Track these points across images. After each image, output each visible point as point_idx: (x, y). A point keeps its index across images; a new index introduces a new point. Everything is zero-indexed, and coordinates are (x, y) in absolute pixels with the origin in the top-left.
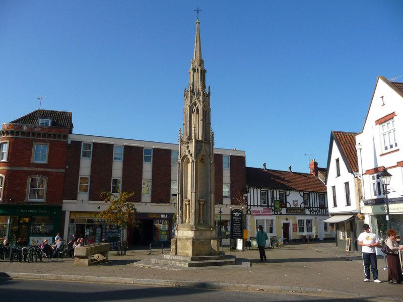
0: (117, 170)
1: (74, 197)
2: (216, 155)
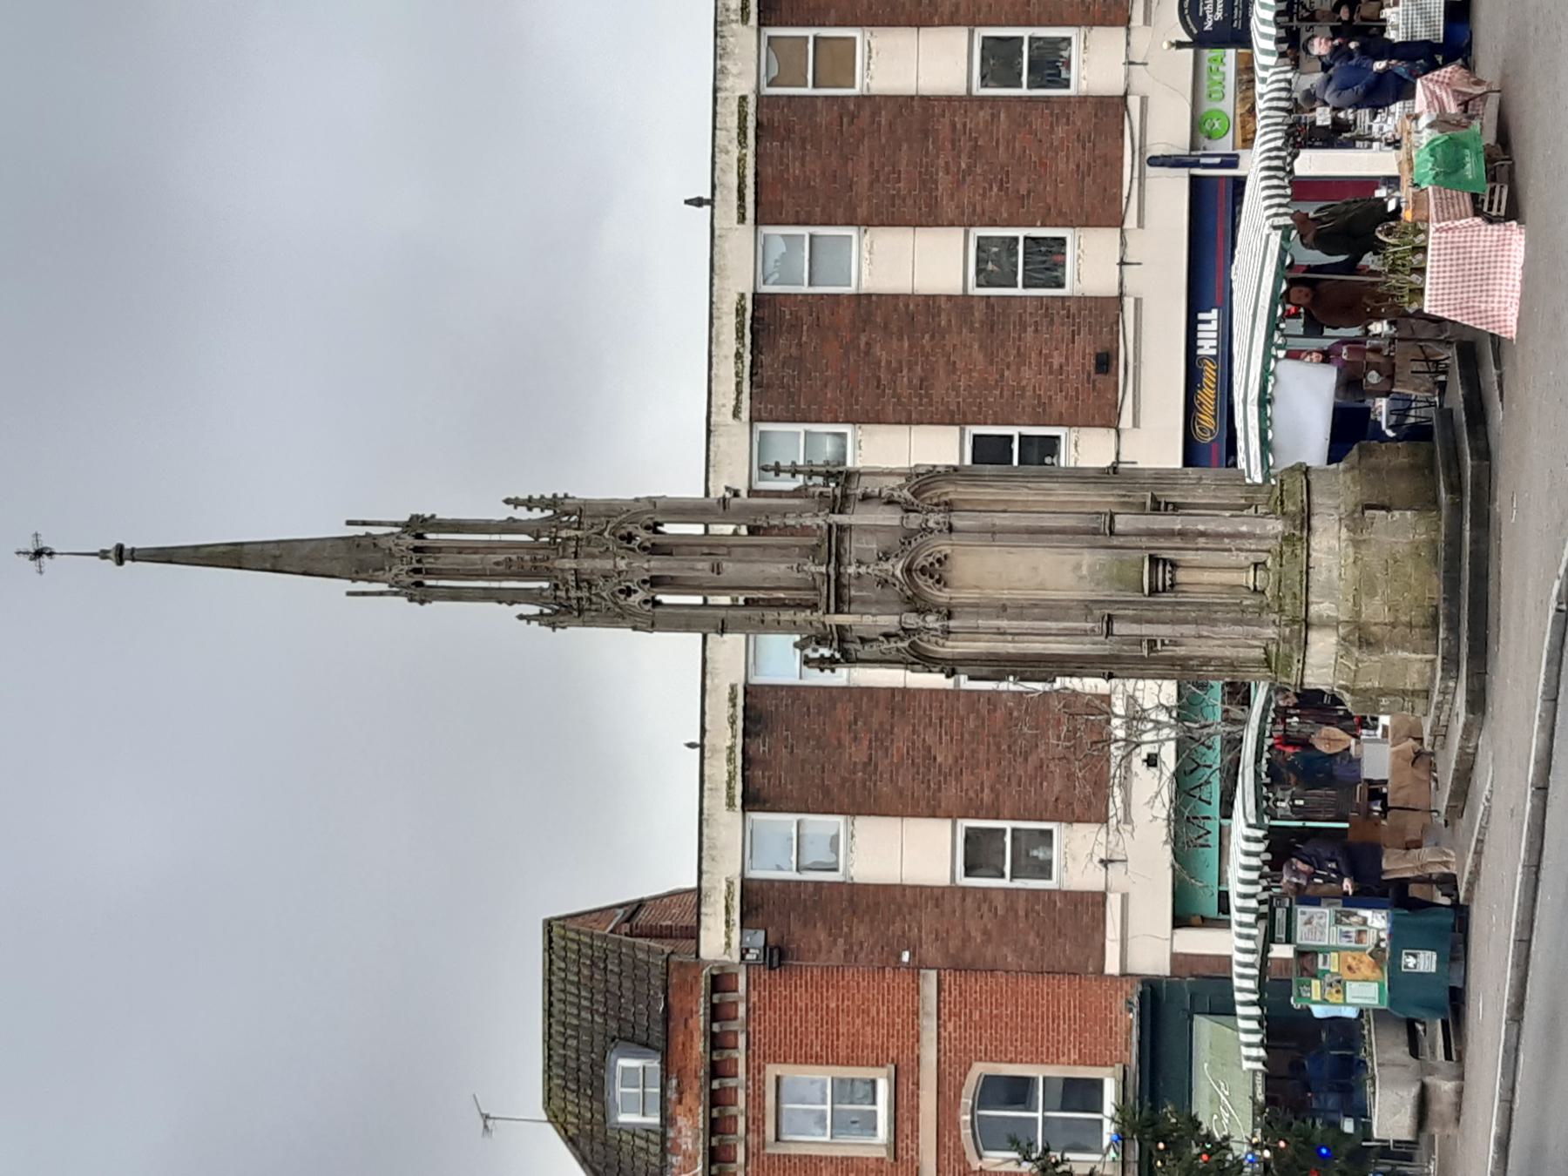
0: (924, 261)
1: (1088, 908)
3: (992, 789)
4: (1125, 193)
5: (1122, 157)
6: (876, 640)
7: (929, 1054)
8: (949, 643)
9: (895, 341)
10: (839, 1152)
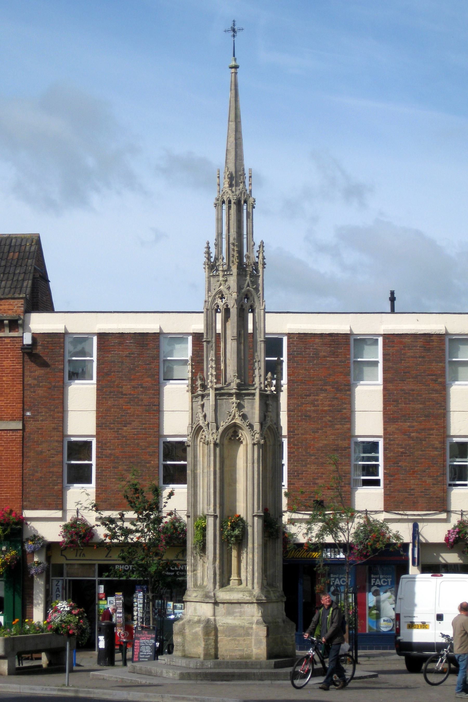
0: (368, 414)
3: (111, 454)
4: (399, 512)
5: (417, 511)
6: (203, 411)
8: (201, 444)
9: (328, 403)
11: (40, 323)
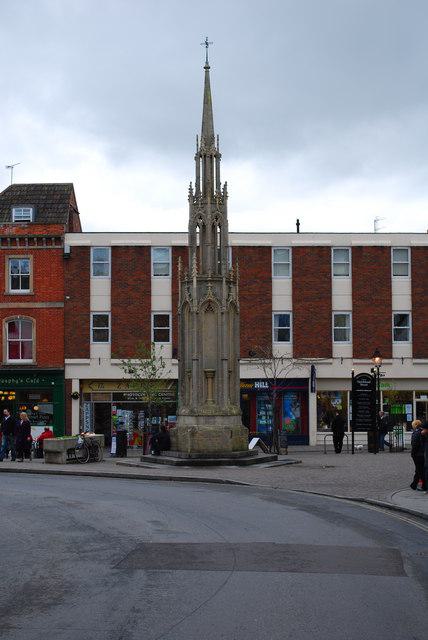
0: (282, 298)
2: (240, 251)
7: (38, 305)
10: (6, 278)
11: (71, 240)
